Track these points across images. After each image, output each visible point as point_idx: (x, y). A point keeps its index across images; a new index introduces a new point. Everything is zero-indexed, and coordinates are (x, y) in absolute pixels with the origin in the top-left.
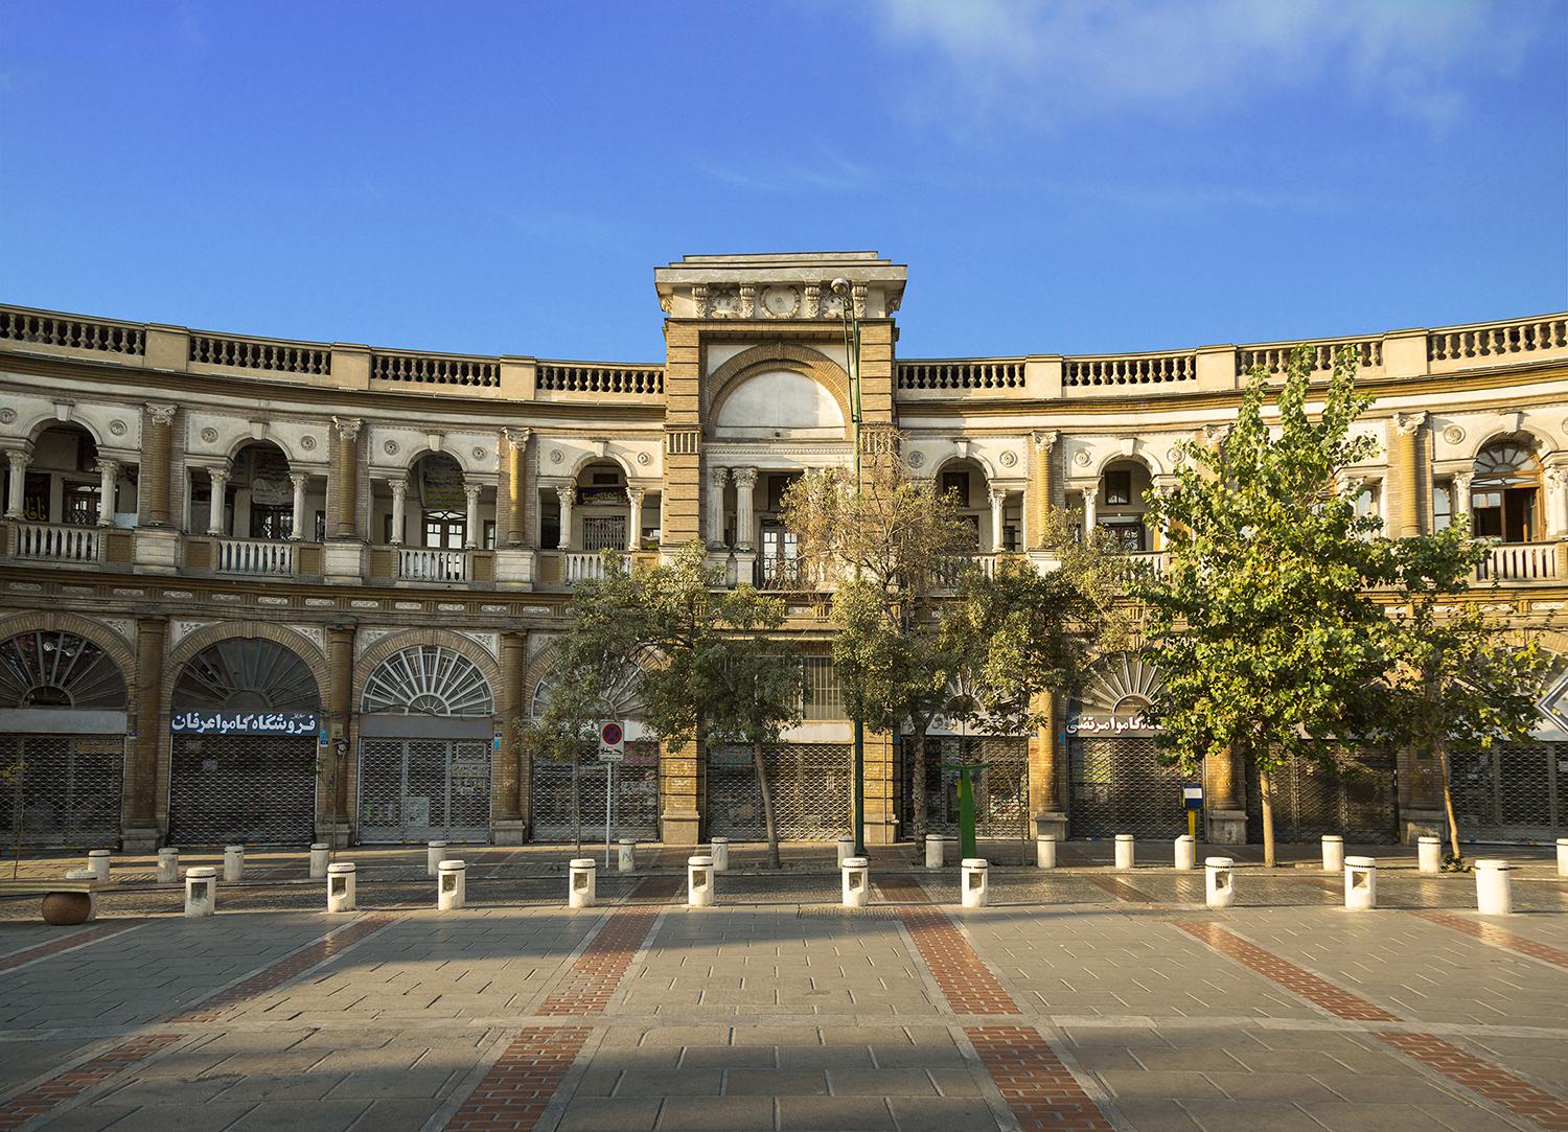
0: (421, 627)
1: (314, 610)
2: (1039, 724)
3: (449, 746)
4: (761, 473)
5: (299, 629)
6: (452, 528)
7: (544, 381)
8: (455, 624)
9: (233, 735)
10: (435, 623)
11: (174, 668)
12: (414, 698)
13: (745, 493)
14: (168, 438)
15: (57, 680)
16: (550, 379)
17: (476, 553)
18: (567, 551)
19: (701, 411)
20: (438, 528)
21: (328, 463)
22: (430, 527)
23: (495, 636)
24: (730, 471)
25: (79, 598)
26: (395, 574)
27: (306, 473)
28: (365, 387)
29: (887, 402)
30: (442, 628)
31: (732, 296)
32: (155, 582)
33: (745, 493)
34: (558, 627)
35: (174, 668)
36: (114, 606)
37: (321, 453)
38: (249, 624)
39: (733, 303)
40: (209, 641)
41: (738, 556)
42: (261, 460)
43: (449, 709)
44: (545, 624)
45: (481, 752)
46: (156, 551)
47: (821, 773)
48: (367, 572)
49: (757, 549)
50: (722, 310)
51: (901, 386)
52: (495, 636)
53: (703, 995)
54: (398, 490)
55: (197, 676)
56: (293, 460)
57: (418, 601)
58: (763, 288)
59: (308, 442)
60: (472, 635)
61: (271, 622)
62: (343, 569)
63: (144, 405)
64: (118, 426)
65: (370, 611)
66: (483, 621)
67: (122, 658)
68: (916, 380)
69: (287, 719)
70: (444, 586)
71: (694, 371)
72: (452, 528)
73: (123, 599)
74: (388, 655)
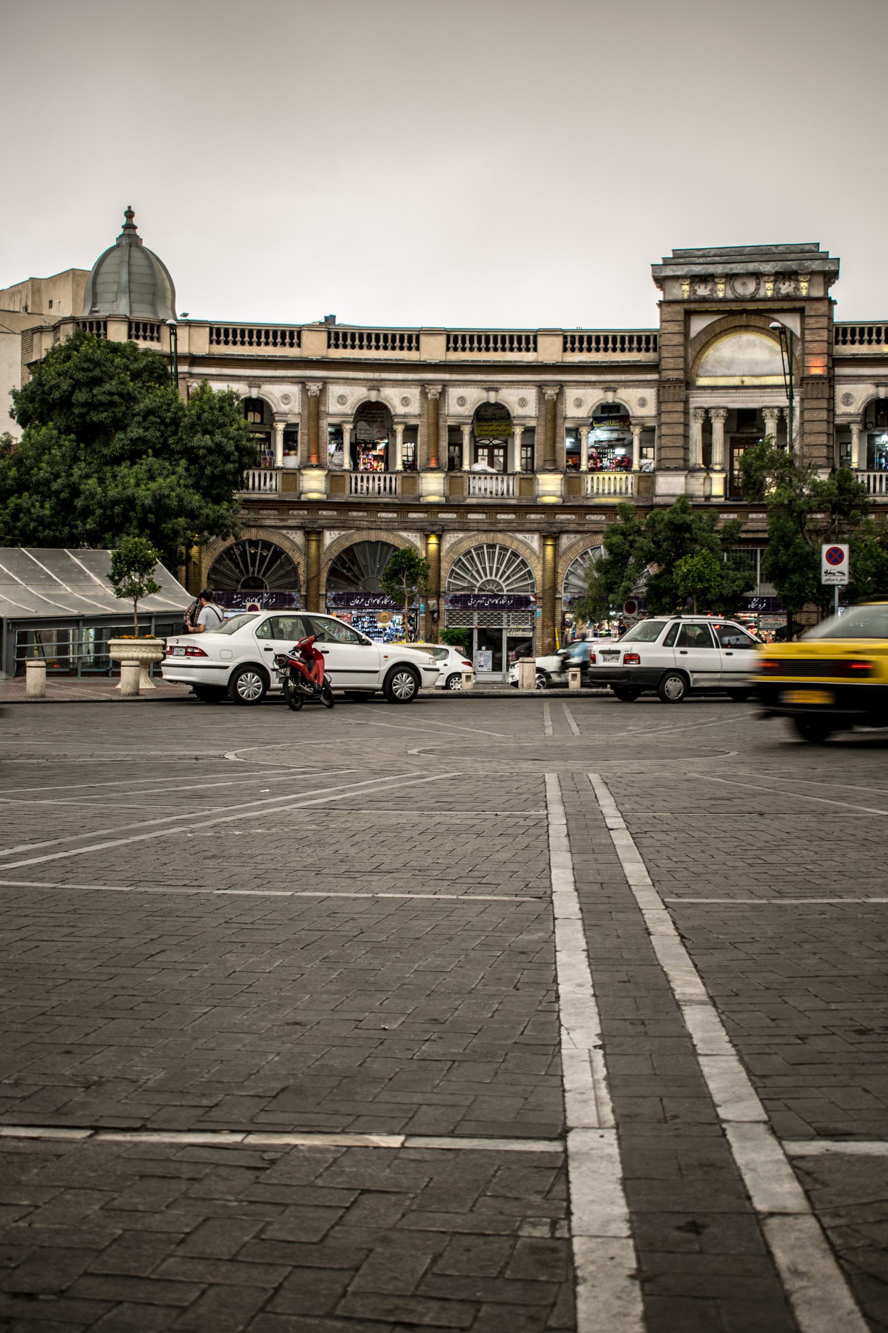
0: (485, 531)
1: (414, 521)
4: (729, 411)
5: (404, 534)
6: (496, 452)
7: (569, 345)
8: (509, 528)
10: (496, 528)
11: (327, 563)
12: (481, 582)
13: (718, 426)
14: (315, 406)
16: (573, 343)
17: (522, 476)
18: (586, 473)
20: (486, 452)
21: (420, 415)
22: (480, 452)
23: (536, 537)
25: (270, 518)
26: (466, 493)
27: (405, 423)
28: (443, 358)
30: (500, 531)
31: (708, 281)
32: (314, 505)
33: (718, 426)
34: (581, 529)
35: (327, 563)
36: (291, 523)
37: (414, 408)
38: (373, 532)
39: (709, 287)
40: (347, 544)
42: (373, 413)
43: (505, 589)
44: (572, 527)
45: (527, 619)
46: (314, 484)
48: (447, 493)
49: (728, 468)
50: (703, 291)
51: (837, 343)
52: (536, 537)
53: (593, 922)
54: (466, 430)
55: (339, 568)
57: (483, 513)
58: (730, 277)
59: (643, 403)
60: (520, 536)
61: (387, 530)
63: (303, 383)
64: (286, 398)
65: (451, 521)
66: (528, 527)
67: (298, 558)
68: (849, 338)
70: (498, 502)
71: (679, 339)
72: (496, 452)
73: (295, 517)
74: (463, 551)
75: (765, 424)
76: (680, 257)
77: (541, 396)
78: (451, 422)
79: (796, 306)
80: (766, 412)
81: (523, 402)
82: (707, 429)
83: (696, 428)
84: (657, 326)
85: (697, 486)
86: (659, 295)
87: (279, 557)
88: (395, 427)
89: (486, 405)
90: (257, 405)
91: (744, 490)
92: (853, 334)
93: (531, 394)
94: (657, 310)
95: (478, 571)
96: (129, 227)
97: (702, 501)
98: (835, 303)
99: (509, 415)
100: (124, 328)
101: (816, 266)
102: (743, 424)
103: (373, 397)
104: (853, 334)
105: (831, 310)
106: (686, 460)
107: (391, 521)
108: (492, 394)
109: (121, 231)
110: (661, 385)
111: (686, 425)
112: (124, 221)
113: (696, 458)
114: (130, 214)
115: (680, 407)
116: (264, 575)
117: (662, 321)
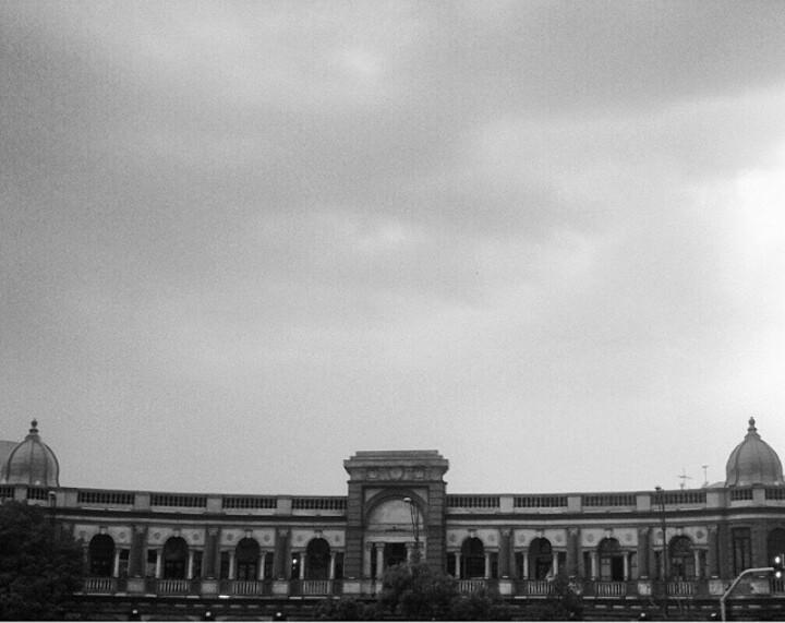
4: (386, 544)
13: (380, 555)
19: (362, 520)
29: (440, 516)
33: (380, 555)
36: (119, 610)
37: (635, 542)
50: (372, 476)
51: (448, 506)
64: (122, 535)
71: (358, 503)
76: (361, 456)
77: (277, 534)
78: (223, 549)
79: (424, 486)
81: (267, 539)
83: (368, 555)
84: (346, 494)
85: (368, 589)
86: (348, 477)
89: (245, 539)
92: (171, 499)
93: (271, 533)
94: (347, 486)
96: (34, 431)
97: (370, 597)
98: (446, 483)
100: (25, 492)
101: (434, 463)
102: (395, 552)
103: (177, 534)
104: (457, 501)
105: (444, 488)
106: (362, 574)
109: (28, 433)
110: (348, 529)
111: (362, 552)
112: (748, 426)
113: (367, 571)
114: (752, 422)
115: (358, 542)
117: (350, 492)
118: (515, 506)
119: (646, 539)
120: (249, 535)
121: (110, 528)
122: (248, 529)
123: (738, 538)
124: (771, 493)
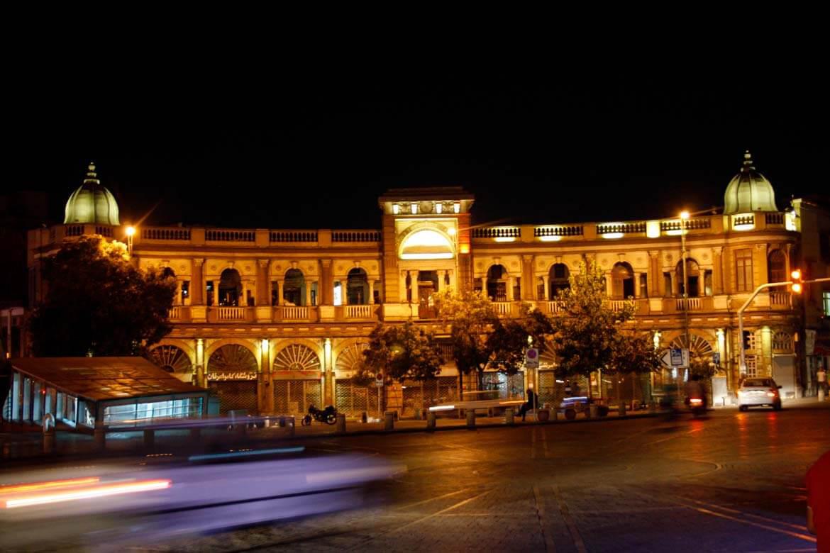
2: (723, 366)
3: (304, 382)
9: (229, 381)
14: (200, 272)
15: (166, 363)
24: (408, 272)
36: (187, 335)
40: (218, 347)
41: (412, 305)
44: (340, 334)
47: (447, 388)
51: (473, 237)
56: (243, 276)
59: (311, 268)
62: (328, 316)
64: (183, 267)
66: (316, 334)
69: (247, 374)
75: (438, 279)
80: (439, 273)
82: (408, 281)
87: (181, 354)
88: (242, 282)
89: (292, 270)
90: (168, 272)
91: (427, 313)
95: (289, 359)
99: (302, 275)
103: (231, 266)
107: (242, 333)
108: (559, 259)
116: (172, 365)
118: (206, 239)
119: (654, 262)
120: (295, 266)
121: (302, 262)
122: (293, 260)
123: (740, 258)
124: (770, 219)
